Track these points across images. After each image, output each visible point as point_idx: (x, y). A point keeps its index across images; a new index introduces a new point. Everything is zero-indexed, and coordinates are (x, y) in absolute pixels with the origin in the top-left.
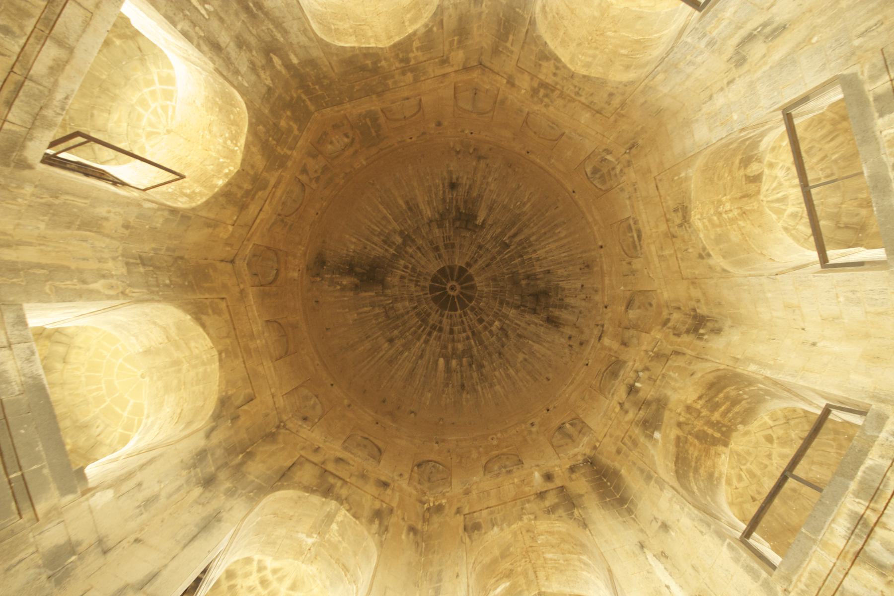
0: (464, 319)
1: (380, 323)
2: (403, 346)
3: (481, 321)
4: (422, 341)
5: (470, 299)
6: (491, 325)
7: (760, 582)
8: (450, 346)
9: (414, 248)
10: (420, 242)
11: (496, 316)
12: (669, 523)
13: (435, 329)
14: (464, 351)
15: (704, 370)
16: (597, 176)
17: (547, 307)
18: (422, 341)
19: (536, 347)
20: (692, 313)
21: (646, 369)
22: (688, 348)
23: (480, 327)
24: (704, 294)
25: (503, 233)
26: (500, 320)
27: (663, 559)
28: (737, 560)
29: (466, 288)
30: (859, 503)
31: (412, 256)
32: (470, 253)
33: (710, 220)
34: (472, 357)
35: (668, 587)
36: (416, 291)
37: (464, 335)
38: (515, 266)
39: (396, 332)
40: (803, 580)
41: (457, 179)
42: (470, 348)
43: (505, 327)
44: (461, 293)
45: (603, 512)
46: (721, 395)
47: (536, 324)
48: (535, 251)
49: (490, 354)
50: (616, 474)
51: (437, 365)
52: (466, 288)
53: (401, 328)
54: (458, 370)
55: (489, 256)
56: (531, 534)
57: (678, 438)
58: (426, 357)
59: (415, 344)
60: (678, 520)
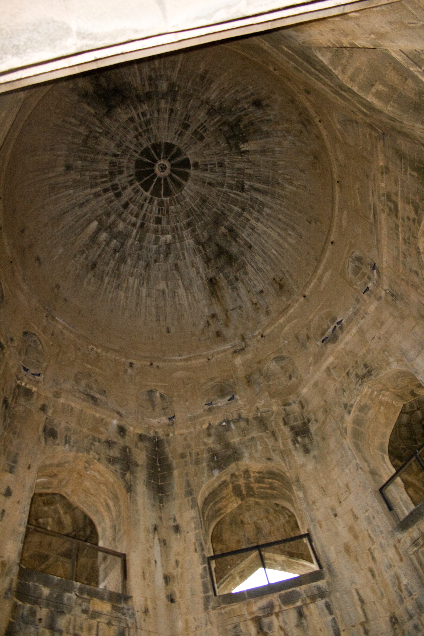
0: (146, 204)
1: (74, 143)
2: (74, 181)
3: (158, 221)
4: (94, 190)
5: (168, 193)
6: (163, 233)
7: (205, 595)
8: (113, 217)
9: (169, 106)
10: (178, 106)
11: (175, 230)
12: (181, 529)
13: (114, 190)
14: (120, 233)
15: (278, 464)
16: (357, 263)
17: (220, 270)
18: (94, 190)
19: (181, 291)
20: (306, 420)
21: (247, 421)
22: (282, 440)
23: (152, 226)
24: (324, 423)
25: (250, 177)
26: (174, 237)
27: (162, 544)
28: (203, 577)
29: (173, 180)
30: (278, 600)
31: (158, 111)
32: (208, 159)
33: (372, 392)
34: (123, 244)
35: (156, 562)
36: (131, 142)
37: (134, 219)
38: (231, 210)
39: (79, 163)
40: (226, 609)
41: (268, 105)
42: (128, 236)
43: (173, 247)
44: (165, 179)
45: (145, 489)
46: (270, 481)
47: (198, 273)
48: (258, 220)
49: (139, 257)
50: (169, 468)
51: (87, 225)
52: (173, 180)
53: (86, 163)
54: (103, 246)
55: (220, 179)
56: (87, 465)
57: (225, 482)
58: (85, 209)
59: (85, 189)
60: (188, 532)
